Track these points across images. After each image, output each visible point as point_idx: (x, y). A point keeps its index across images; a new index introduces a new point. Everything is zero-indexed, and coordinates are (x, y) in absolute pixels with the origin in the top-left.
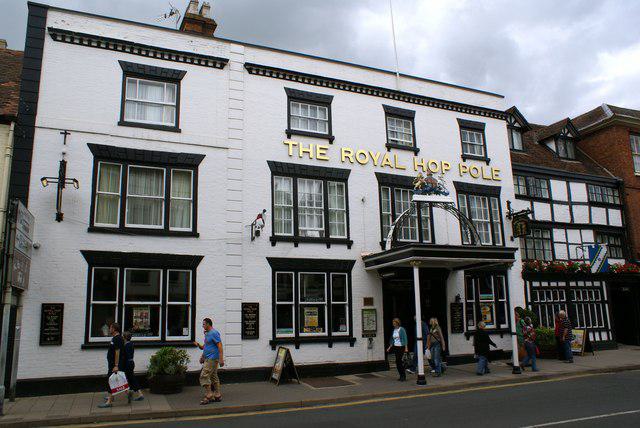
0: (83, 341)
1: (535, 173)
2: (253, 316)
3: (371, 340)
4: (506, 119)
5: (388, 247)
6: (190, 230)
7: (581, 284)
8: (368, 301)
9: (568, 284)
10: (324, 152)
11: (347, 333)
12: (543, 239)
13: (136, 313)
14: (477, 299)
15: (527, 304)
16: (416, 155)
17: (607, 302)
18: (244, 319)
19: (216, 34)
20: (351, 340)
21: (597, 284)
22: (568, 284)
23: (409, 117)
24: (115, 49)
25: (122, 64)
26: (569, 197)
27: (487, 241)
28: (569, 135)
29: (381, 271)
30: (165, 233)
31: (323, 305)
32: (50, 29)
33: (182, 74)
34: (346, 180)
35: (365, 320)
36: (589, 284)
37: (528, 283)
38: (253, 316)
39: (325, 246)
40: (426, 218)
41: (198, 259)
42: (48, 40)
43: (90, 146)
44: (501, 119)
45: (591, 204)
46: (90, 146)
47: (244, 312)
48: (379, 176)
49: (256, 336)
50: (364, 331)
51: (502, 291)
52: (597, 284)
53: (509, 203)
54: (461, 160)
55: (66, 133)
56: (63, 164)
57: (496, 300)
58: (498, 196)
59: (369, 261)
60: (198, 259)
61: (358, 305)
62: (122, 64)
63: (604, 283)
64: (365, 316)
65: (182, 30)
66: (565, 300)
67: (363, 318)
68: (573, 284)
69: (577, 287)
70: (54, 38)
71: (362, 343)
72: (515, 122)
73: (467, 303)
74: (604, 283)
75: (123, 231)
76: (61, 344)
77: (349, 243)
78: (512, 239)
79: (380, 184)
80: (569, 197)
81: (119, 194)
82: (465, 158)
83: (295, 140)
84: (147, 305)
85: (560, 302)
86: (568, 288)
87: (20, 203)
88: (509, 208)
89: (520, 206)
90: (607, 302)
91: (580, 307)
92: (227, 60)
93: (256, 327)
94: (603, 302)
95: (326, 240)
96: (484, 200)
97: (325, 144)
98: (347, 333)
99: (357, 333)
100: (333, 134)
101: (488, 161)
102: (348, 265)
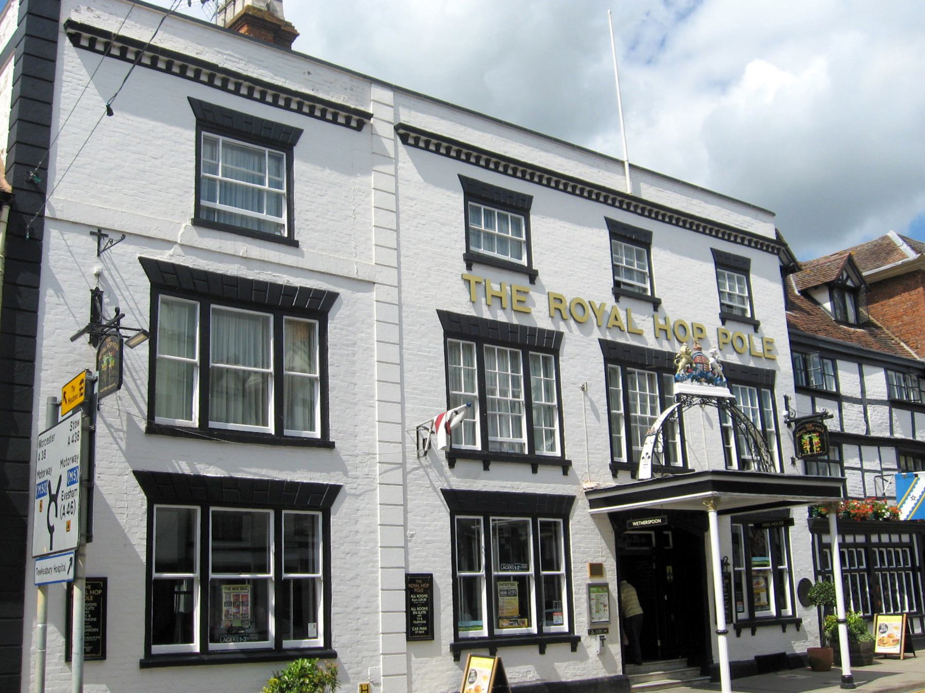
0: (141, 654)
1: (887, 362)
2: (423, 598)
3: (602, 640)
4: (778, 254)
5: (645, 472)
6: (317, 434)
7: (885, 538)
8: (596, 570)
9: (868, 539)
10: (522, 298)
11: (565, 628)
12: (829, 461)
13: (226, 594)
14: (749, 565)
15: (817, 573)
16: (656, 309)
17: (919, 569)
18: (410, 604)
19: (296, 46)
20: (573, 641)
21: (905, 538)
22: (868, 539)
23: (643, 240)
24: (182, 74)
25: (194, 103)
26: (863, 392)
27: (552, 448)
28: (849, 283)
29: (612, 516)
30: (279, 440)
31: (265, 581)
32: (70, 24)
33: (298, 133)
34: (556, 352)
35: (593, 602)
36: (895, 538)
37: (816, 536)
38: (423, 598)
39: (528, 469)
40: (549, 409)
41: (333, 491)
42: (65, 45)
43: (142, 260)
44: (772, 253)
45: (893, 403)
46: (142, 260)
47: (409, 591)
48: (605, 345)
49: (429, 634)
50: (592, 623)
51: (779, 551)
52: (905, 538)
53: (786, 399)
54: (719, 323)
55: (99, 234)
56: (97, 295)
57: (774, 566)
58: (771, 387)
59: (598, 498)
60: (333, 491)
61: (581, 577)
62: (194, 103)
63: (914, 536)
64: (593, 596)
65: (233, 29)
66: (864, 566)
67: (590, 599)
68: (874, 539)
69: (880, 544)
70: (75, 41)
71: (591, 645)
72: (848, 277)
73: (735, 571)
74: (914, 536)
75: (205, 433)
76: (103, 657)
77: (564, 465)
78: (793, 463)
79: (607, 360)
80: (863, 392)
81: (476, 393)
82: (471, 259)
83: (479, 272)
84: (242, 581)
85: (858, 570)
86: (867, 546)
87: (920, 462)
88: (787, 408)
89: (801, 406)
90: (919, 569)
91: (884, 576)
92: (369, 116)
93: (429, 618)
94: (914, 569)
95: (535, 462)
96: (514, 356)
97: (522, 281)
98: (320, 642)
99: (581, 629)
100: (757, 318)
101: (532, 276)
102: (563, 505)
